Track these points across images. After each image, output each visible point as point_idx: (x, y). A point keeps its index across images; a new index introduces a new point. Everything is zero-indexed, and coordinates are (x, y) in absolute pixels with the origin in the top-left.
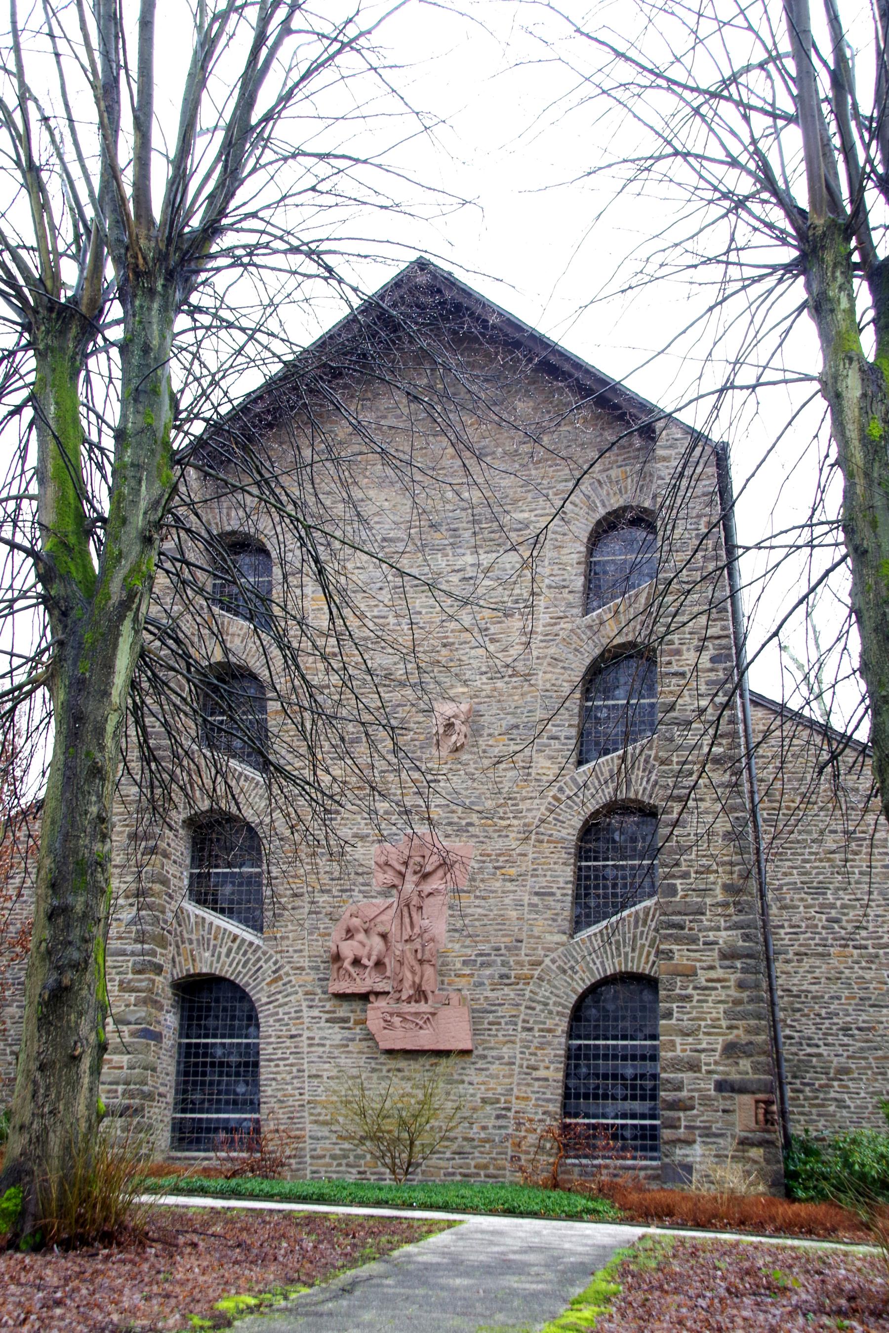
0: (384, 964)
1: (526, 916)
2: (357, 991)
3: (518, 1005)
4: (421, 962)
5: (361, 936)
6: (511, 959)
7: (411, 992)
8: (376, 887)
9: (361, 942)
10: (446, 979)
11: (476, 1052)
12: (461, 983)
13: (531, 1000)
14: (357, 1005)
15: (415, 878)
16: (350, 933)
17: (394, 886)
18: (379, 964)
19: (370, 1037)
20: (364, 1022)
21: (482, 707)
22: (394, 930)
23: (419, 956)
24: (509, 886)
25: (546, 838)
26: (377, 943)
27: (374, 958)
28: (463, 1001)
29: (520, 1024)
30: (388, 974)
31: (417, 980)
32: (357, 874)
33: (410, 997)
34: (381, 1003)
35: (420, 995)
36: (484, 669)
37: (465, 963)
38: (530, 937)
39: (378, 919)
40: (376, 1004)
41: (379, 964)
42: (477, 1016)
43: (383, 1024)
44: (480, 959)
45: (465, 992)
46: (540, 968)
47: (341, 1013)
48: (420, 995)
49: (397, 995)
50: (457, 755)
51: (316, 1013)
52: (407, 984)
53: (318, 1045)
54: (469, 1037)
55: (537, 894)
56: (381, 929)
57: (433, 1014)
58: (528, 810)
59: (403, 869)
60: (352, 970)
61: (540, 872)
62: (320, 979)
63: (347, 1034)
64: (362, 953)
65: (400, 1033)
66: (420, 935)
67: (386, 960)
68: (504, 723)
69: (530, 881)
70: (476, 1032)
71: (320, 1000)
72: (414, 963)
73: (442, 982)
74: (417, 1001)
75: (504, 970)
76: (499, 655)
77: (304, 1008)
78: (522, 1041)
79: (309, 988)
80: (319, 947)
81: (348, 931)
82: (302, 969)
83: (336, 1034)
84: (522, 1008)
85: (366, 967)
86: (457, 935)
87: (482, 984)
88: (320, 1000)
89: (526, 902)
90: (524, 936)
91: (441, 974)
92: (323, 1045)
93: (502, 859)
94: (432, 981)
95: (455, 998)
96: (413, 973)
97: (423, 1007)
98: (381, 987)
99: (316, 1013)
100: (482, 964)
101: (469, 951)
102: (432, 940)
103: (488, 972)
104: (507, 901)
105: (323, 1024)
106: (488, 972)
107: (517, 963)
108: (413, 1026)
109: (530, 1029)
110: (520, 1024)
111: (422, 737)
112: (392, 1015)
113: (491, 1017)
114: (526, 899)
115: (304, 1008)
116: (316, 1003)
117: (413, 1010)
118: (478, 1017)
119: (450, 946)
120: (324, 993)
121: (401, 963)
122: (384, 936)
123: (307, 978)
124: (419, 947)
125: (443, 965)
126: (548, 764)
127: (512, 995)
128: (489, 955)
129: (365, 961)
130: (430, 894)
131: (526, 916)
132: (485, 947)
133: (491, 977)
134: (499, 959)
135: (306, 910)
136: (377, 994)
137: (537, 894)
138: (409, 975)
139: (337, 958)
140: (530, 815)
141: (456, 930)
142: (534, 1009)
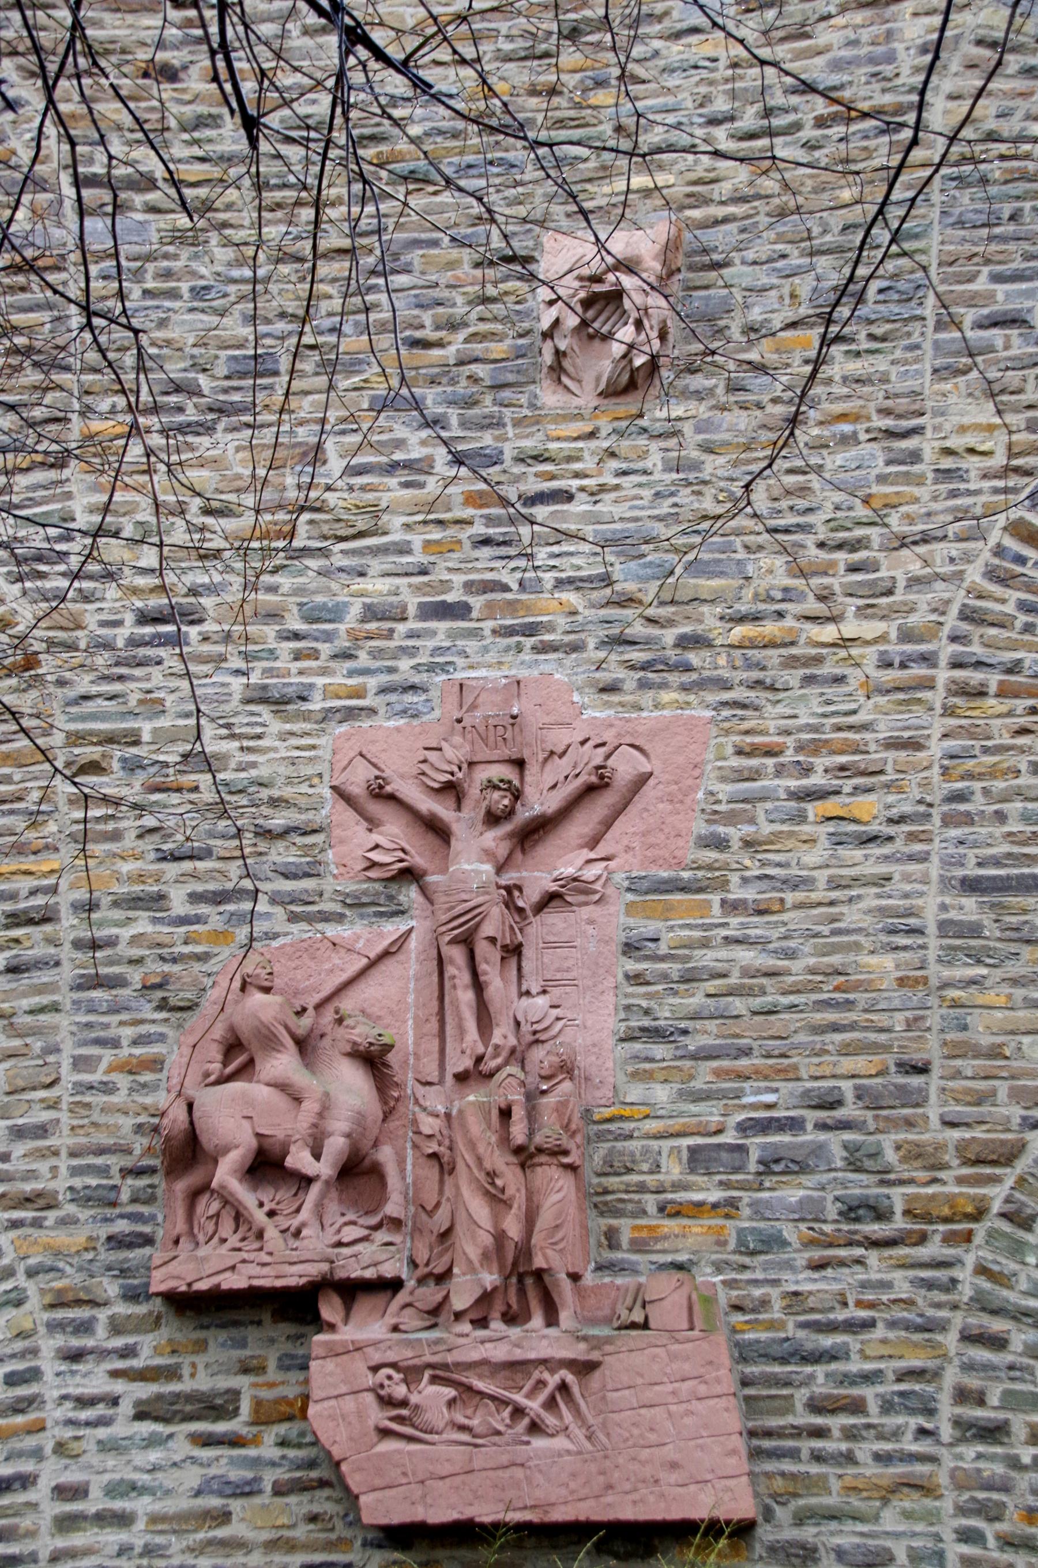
0: (376, 1172)
1: (936, 972)
2: (267, 1280)
3: (928, 1327)
4: (525, 1156)
5: (283, 1063)
6: (887, 1142)
7: (490, 1279)
8: (338, 881)
9: (282, 1087)
10: (626, 1227)
11: (765, 1533)
12: (690, 1237)
13: (983, 1304)
14: (265, 1342)
15: (493, 838)
16: (239, 1055)
17: (409, 874)
18: (358, 1173)
19: (322, 1475)
20: (298, 1410)
21: (722, 238)
22: (408, 1038)
23: (518, 1132)
24: (865, 861)
25: (993, 680)
26: (350, 1087)
27: (336, 1145)
28: (698, 1312)
29: (947, 1409)
30: (393, 1208)
31: (513, 1229)
32: (266, 834)
33: (486, 1298)
34: (367, 1328)
35: (526, 1287)
36: (721, 105)
37: (696, 1158)
38: (958, 1051)
39: (347, 1004)
40: (347, 1333)
41: (358, 1173)
42: (762, 1372)
43: (378, 1416)
44: (756, 1143)
45: (707, 1276)
46: (1010, 1176)
47: (200, 1379)
48: (526, 1287)
49: (431, 1295)
50: (628, 405)
51: (95, 1379)
52: (471, 1245)
53: (102, 1519)
54: (740, 1463)
55: (971, 886)
56: (362, 1033)
57: (585, 1368)
58: (915, 582)
59: (441, 809)
60: (246, 1196)
61: (978, 804)
62: (116, 1242)
63: (223, 1463)
64: (289, 1125)
65: (446, 1452)
66: (516, 1056)
67: (386, 1155)
68: (805, 285)
69: (943, 840)
70: (761, 1443)
71: (116, 1328)
72: (500, 1161)
73: (611, 1238)
74: (510, 1319)
75: (862, 1186)
76: (781, 52)
77: (49, 1365)
78: (961, 1482)
79: (71, 1279)
80: (124, 1117)
81: (233, 1046)
82: (42, 1201)
83: (176, 1468)
84: (950, 1340)
85: (306, 1181)
86: (659, 1051)
87: (773, 1242)
88: (116, 1328)
89: (930, 920)
90: (932, 1049)
91: (601, 1202)
92: (123, 1520)
93: (820, 762)
94: (570, 1231)
95: (669, 1299)
96: (497, 1199)
97: (537, 1340)
98: (372, 1257)
99: (95, 1379)
100: (768, 1164)
101: (711, 1113)
102: (566, 1069)
103: (793, 1195)
104: (852, 916)
105: (123, 1428)
106: (793, 1195)
107: (914, 1154)
108: (501, 1419)
109: (993, 1433)
110: (947, 1409)
111: (497, 349)
112: (411, 1374)
113: (820, 1379)
114: (930, 908)
115: (49, 1365)
116: (101, 1337)
117: (499, 1353)
118: (775, 1383)
119: (635, 1093)
120: (132, 1296)
121: (443, 1165)
122: (373, 1060)
123: (61, 1238)
124: (516, 1097)
125: (610, 1169)
126: (985, 413)
127: (902, 1283)
128: (794, 1125)
129: (300, 1159)
130: (550, 899)
131: (936, 972)
132: (779, 1097)
133: (808, 1213)
134: (835, 1142)
135: (67, 973)
136: (352, 1291)
137: (971, 886)
138: (479, 1209)
139: (187, 1151)
140: (923, 599)
141: (655, 1034)
142: (998, 1343)
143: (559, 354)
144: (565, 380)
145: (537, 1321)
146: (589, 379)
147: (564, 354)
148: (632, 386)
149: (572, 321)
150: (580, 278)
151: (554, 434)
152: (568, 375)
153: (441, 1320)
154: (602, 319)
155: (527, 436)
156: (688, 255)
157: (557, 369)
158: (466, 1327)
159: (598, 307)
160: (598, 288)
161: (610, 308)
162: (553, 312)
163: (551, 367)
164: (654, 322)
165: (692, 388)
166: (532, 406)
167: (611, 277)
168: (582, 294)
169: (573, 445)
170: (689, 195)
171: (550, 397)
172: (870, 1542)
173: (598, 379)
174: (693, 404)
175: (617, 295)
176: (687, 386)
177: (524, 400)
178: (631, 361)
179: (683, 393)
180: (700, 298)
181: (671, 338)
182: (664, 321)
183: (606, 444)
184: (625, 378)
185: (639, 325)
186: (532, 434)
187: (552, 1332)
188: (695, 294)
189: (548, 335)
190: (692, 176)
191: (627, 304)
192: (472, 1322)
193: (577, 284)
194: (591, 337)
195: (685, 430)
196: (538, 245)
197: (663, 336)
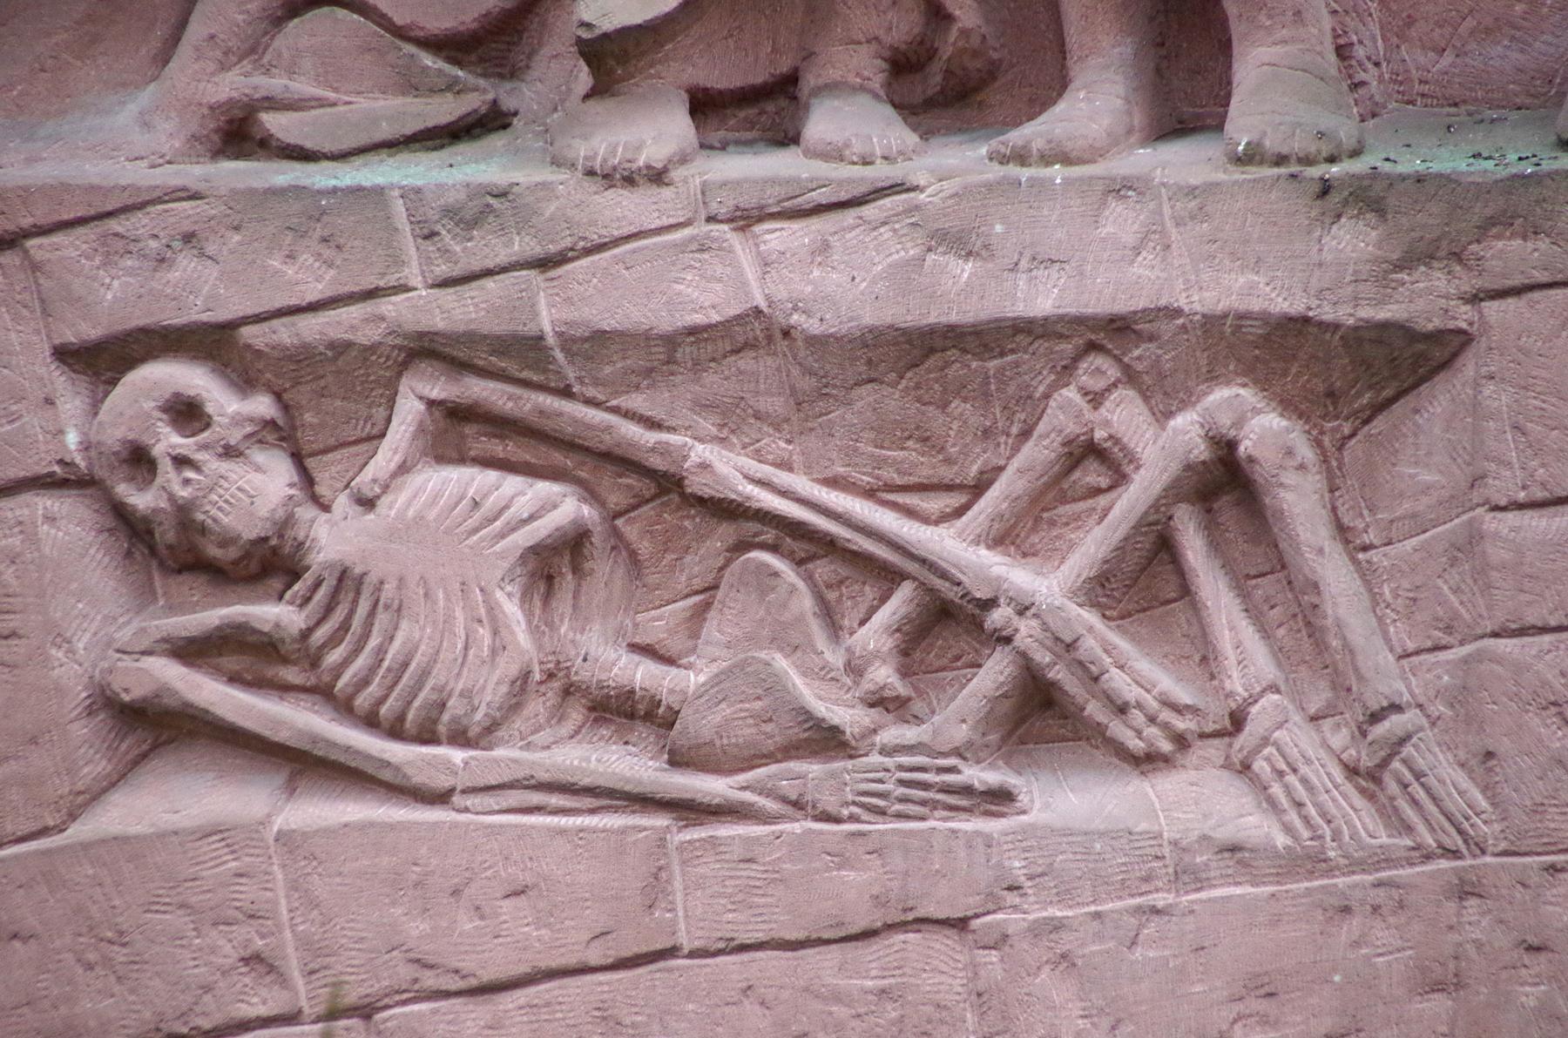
145: (1097, 99)
153: (521, 96)
158: (656, 129)
187: (1185, 162)
192: (703, 105)
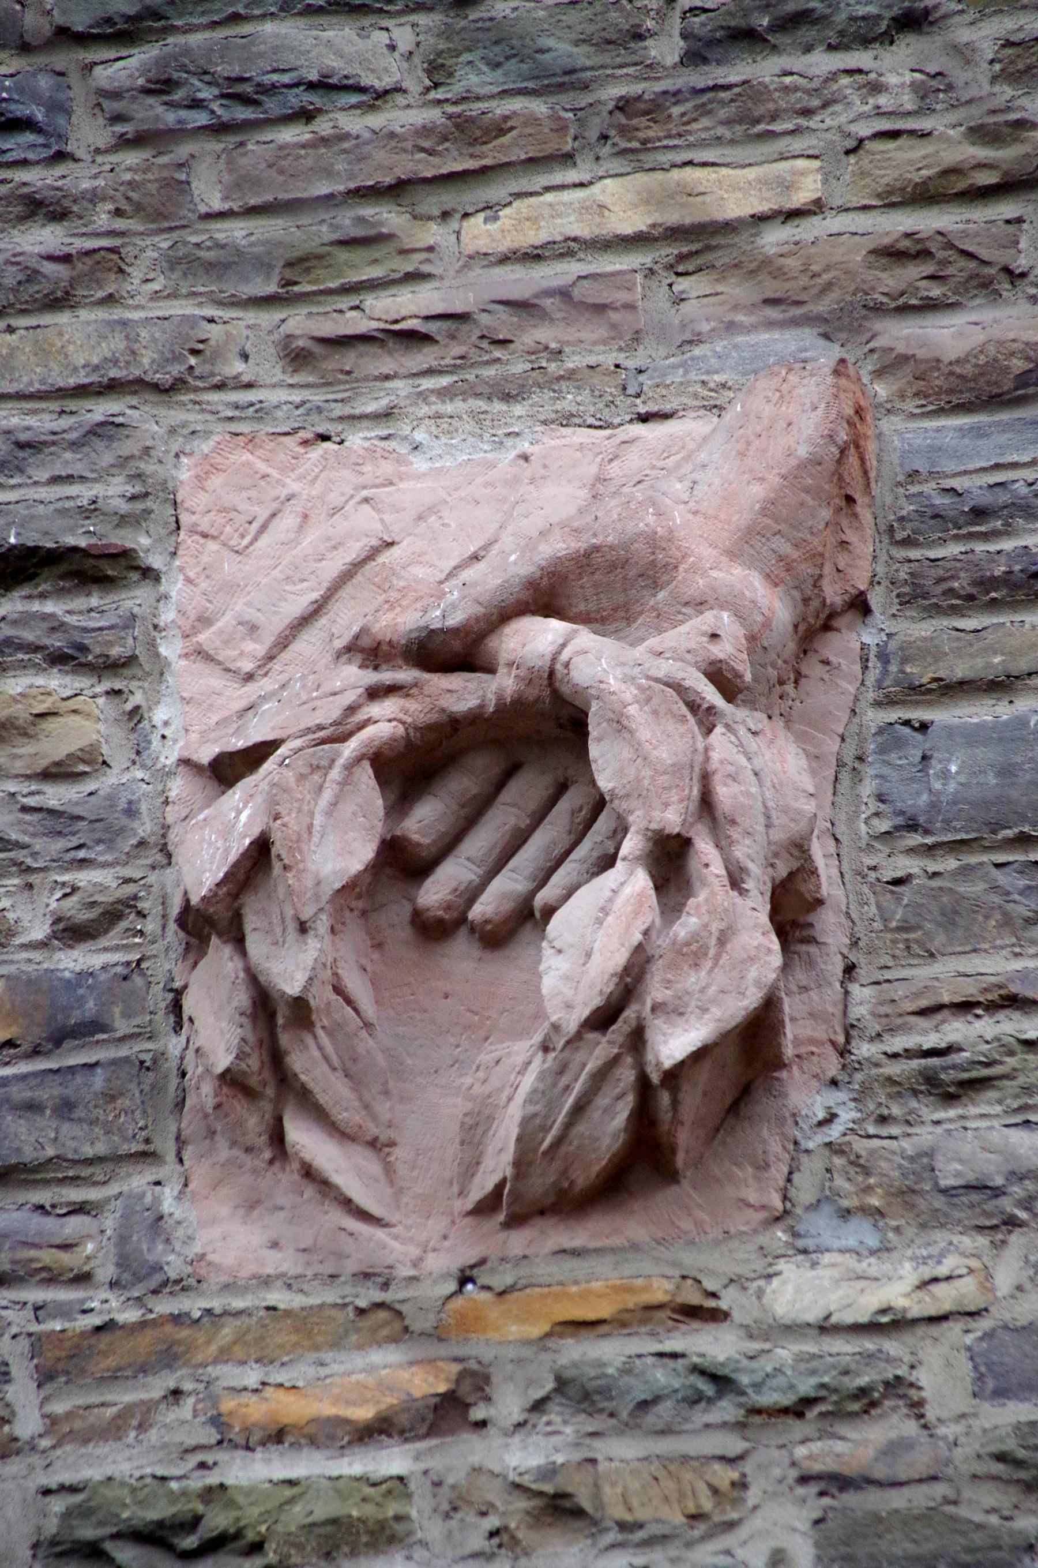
143: (270, 1014)
144: (304, 1138)
146: (427, 1122)
147: (301, 1011)
148: (644, 1162)
149: (337, 846)
150: (369, 651)
151: (257, 1410)
152: (320, 1116)
154: (482, 841)
155: (114, 1430)
156: (899, 535)
157: (269, 1081)
159: (461, 784)
160: (461, 693)
161: (525, 791)
162: (238, 815)
163: (231, 1080)
164: (747, 851)
165: (950, 1172)
166: (136, 1274)
167: (536, 638)
168: (385, 722)
169: (355, 1464)
170: (893, 254)
171: (224, 1233)
172: (960, 1111)
173: (474, 1130)
174: (958, 1251)
175: (553, 726)
176: (925, 1161)
177: (95, 1246)
178: (637, 1039)
179: (905, 1195)
180: (974, 736)
181: (831, 928)
182: (800, 847)
183: (523, 1457)
184: (611, 1124)
185: (669, 862)
186: (141, 1417)
188: (942, 716)
189: (211, 923)
190: (908, 161)
191: (608, 763)
193: (355, 677)
194: (433, 930)
195: (928, 1380)
196: (154, 499)
197: (792, 913)
